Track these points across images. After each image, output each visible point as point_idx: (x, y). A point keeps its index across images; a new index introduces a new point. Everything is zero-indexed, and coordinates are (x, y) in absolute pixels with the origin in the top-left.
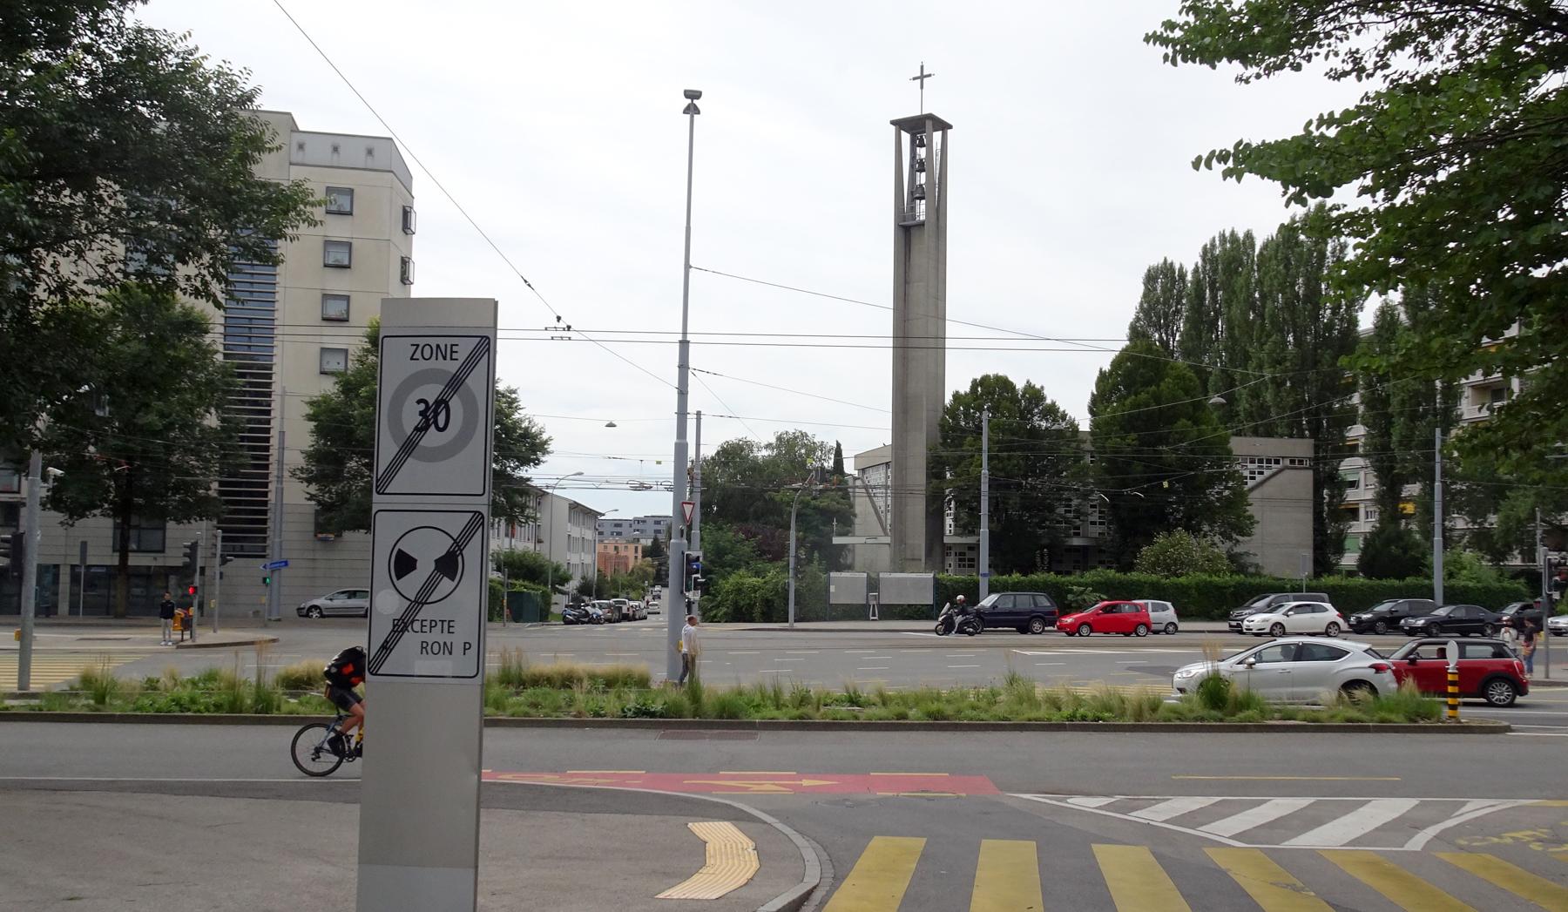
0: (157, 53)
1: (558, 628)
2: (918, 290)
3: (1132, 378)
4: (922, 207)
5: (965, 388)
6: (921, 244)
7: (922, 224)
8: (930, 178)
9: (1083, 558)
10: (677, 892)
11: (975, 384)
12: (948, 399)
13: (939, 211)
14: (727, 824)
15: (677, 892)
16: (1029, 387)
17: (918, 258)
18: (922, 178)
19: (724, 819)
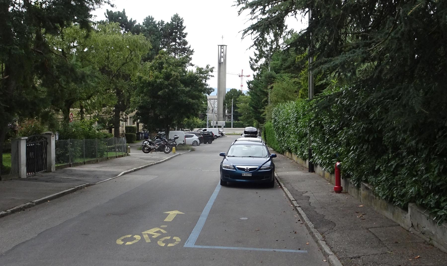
0: (150, 82)
1: (232, 128)
2: (221, 73)
3: (254, 86)
4: (222, 60)
5: (229, 90)
6: (222, 66)
7: (222, 63)
8: (224, 54)
9: (380, 56)
10: (181, 213)
11: (231, 90)
12: (227, 92)
13: (225, 60)
14: (307, 26)
15: (181, 213)
16: (240, 90)
17: (221, 68)
18: (222, 55)
19: (310, 25)
